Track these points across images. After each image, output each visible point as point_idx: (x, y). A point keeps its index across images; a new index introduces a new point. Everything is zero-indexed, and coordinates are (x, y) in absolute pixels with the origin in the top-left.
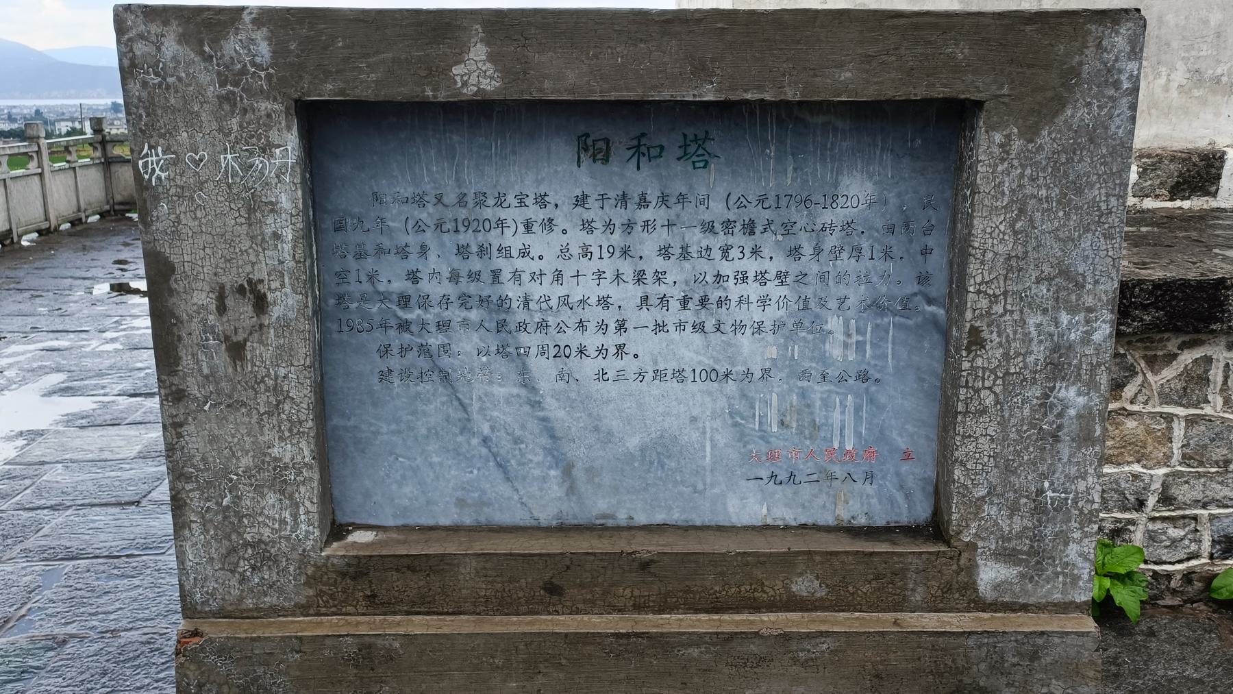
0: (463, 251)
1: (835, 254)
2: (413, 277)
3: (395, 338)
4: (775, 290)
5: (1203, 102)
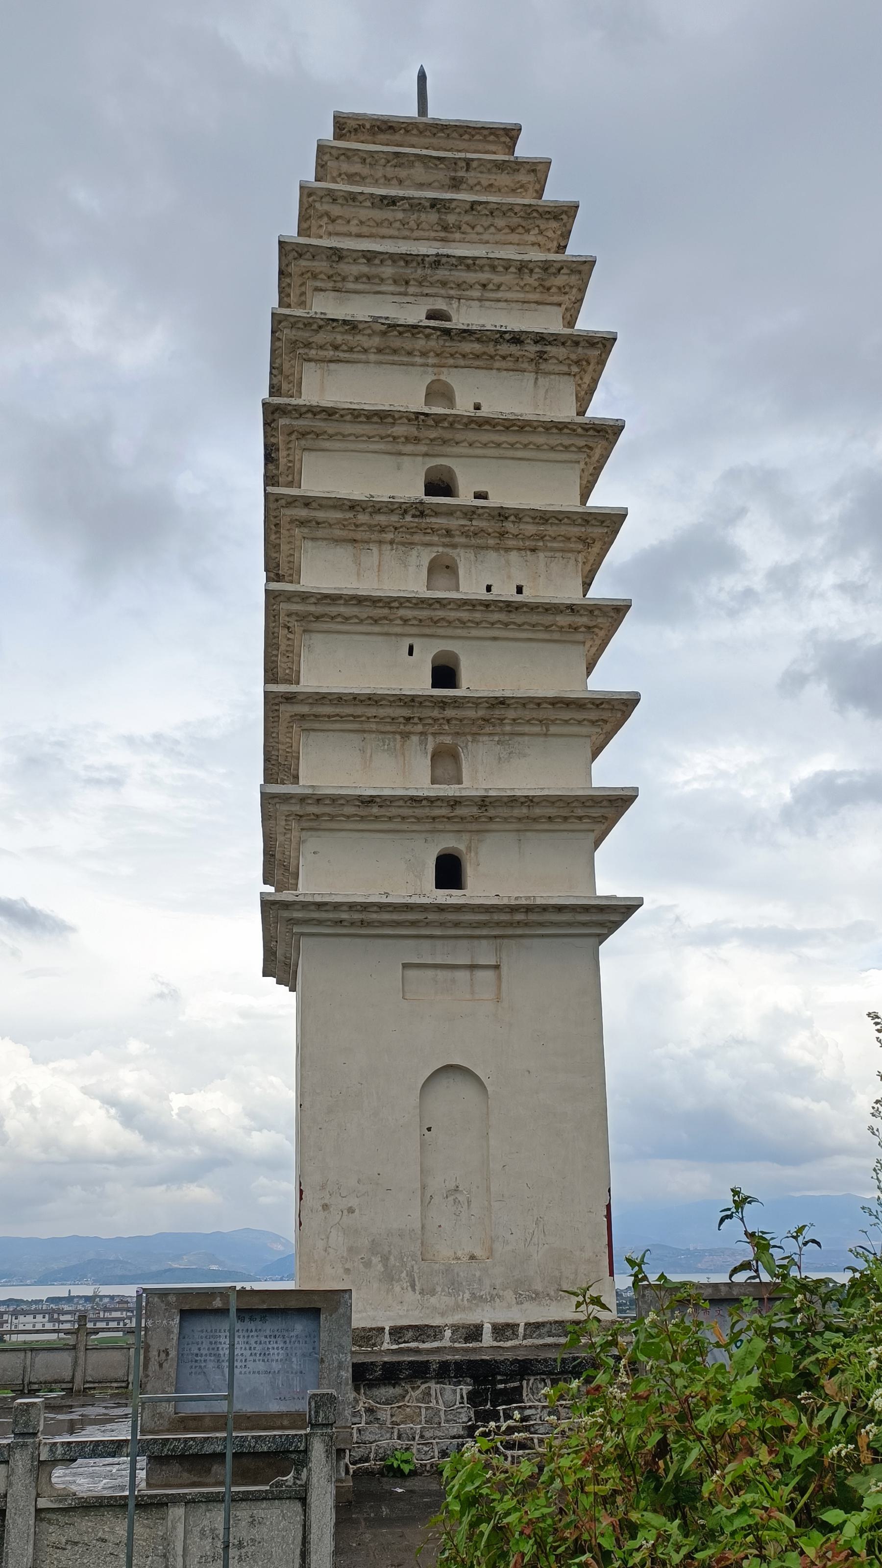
0: (211, 1343)
1: (294, 1343)
2: (199, 1349)
3: (194, 1364)
4: (281, 1352)
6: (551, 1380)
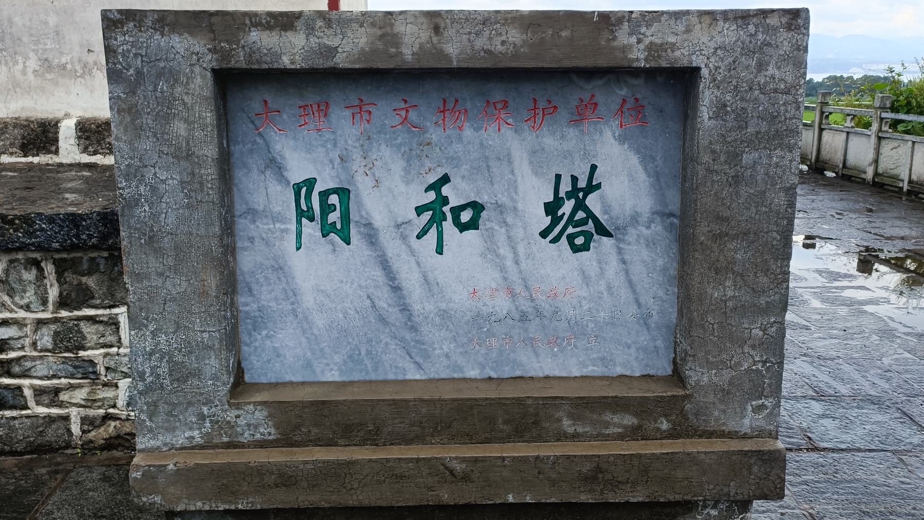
5: (56, 83)
6: (56, 263)
